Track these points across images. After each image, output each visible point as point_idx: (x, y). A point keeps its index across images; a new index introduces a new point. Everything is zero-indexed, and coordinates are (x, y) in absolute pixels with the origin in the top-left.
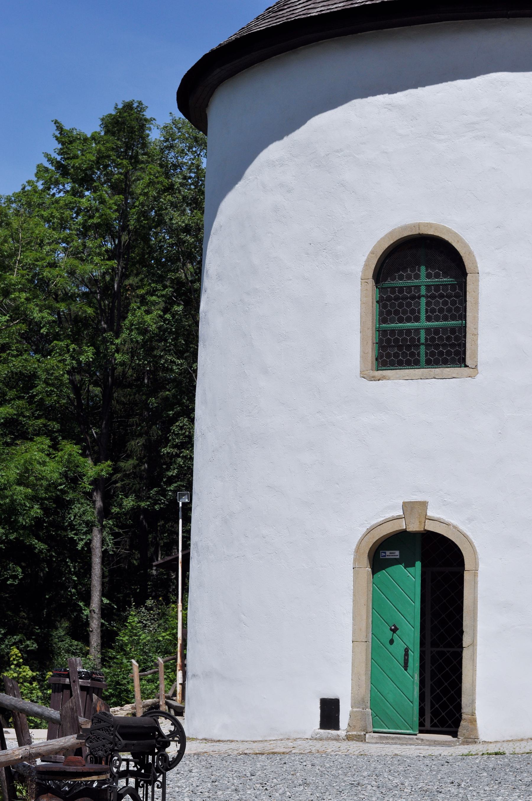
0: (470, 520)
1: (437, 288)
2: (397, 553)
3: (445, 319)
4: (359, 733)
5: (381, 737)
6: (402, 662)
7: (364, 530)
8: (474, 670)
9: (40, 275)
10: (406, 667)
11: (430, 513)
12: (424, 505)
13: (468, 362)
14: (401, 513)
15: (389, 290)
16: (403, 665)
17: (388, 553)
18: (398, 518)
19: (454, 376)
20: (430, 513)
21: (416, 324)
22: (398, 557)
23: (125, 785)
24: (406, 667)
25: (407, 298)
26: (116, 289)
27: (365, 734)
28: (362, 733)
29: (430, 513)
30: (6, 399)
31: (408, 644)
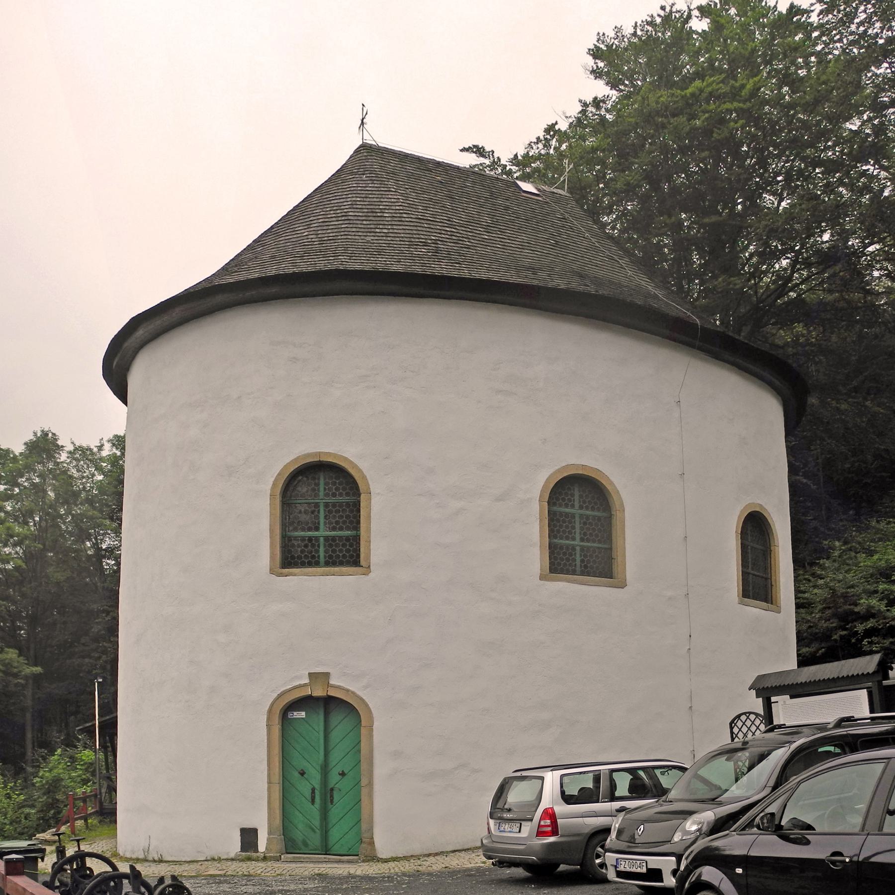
0: (366, 687)
1: (334, 505)
2: (303, 713)
3: (341, 529)
4: (275, 855)
5: (294, 857)
6: (309, 798)
7: (275, 695)
8: (372, 803)
9: (64, 525)
10: (313, 801)
11: (332, 682)
12: (327, 675)
13: (362, 562)
14: (307, 681)
15: (330, 504)
16: (310, 800)
17: (295, 713)
18: (305, 685)
19: (350, 573)
20: (333, 682)
21: (317, 533)
22: (304, 717)
23: (77, 850)
24: (313, 801)
25: (336, 512)
26: (820, 750)
27: (280, 856)
28: (278, 855)
29: (332, 682)
30: (664, 44)
31: (314, 785)
